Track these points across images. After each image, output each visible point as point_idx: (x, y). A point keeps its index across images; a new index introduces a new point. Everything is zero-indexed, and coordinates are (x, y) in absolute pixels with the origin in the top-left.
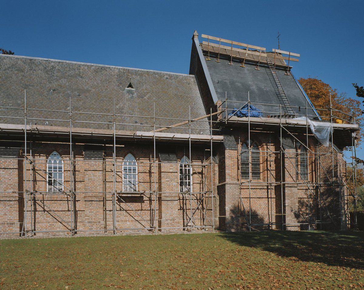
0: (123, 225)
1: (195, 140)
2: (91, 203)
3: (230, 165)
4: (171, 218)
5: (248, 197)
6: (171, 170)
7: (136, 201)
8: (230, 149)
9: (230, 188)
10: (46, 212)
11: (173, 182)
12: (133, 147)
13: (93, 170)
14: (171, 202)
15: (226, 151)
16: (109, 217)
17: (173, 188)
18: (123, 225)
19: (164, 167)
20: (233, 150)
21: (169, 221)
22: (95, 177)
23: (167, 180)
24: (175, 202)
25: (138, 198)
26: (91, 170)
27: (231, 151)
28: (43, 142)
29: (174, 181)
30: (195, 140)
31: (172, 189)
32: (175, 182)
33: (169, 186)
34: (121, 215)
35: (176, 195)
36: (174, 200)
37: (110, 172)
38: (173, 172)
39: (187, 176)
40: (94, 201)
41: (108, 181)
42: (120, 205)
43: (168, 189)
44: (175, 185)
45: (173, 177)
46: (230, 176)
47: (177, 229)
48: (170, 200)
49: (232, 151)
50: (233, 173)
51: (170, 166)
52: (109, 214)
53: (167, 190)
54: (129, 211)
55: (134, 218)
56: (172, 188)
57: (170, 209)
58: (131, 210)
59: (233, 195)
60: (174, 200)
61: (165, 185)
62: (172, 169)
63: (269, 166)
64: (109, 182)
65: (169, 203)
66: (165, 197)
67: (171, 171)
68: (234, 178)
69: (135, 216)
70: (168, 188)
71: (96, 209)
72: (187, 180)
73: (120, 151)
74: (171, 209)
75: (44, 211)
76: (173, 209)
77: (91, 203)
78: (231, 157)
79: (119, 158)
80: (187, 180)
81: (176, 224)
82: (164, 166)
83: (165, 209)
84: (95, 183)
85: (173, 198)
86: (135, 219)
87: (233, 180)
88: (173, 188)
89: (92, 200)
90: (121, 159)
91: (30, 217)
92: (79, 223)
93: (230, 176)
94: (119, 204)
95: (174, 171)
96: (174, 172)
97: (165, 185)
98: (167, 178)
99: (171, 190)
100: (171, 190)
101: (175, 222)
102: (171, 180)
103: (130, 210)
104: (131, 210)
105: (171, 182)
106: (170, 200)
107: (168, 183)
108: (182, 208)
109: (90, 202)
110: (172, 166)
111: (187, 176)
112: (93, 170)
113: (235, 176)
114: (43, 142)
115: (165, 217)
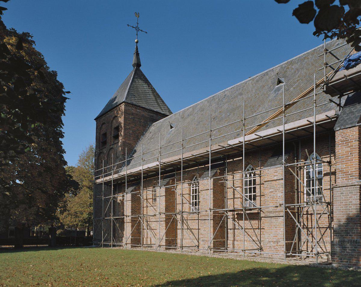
0: (241, 245)
1: (321, 123)
2: (204, 222)
3: (344, 155)
4: (275, 240)
5: (128, 223)
6: (275, 177)
7: (254, 218)
8: (343, 127)
9: (341, 193)
10: (189, 230)
11: (277, 192)
12: (251, 157)
13: (206, 190)
14: (275, 219)
15: (337, 134)
16: (230, 235)
17: (278, 200)
18: (241, 245)
19: (268, 175)
20: (350, 128)
21: (272, 243)
22: (207, 196)
23: (270, 190)
24: (279, 218)
25: (256, 215)
26: (205, 190)
27: (345, 131)
28: (187, 170)
29: (278, 191)
30: (321, 123)
31: (277, 202)
32: (280, 193)
33: (274, 199)
34: (241, 234)
35: (281, 209)
36: (278, 217)
37: (230, 189)
38: (278, 180)
39: (311, 181)
40: (206, 220)
41: (229, 198)
42: (238, 223)
43: (272, 203)
44: (279, 197)
45: (277, 186)
46: (345, 173)
47: (281, 255)
48: (274, 217)
49: (349, 130)
50: (351, 167)
51: (274, 172)
52: (230, 233)
53: (270, 204)
54: (247, 230)
55: (251, 238)
56: (276, 200)
57: (274, 228)
58: (249, 229)
59: (346, 205)
60: (278, 217)
61: (268, 198)
62: (276, 176)
63: (237, 181)
64: (230, 199)
65: (273, 220)
66: (268, 213)
67: (275, 178)
68: (351, 176)
69: (253, 236)
70: (272, 201)
71: (208, 228)
72: (195, 202)
73: (238, 164)
74: (275, 228)
75: (188, 229)
76: (277, 228)
77: (204, 222)
78: (346, 142)
79: (238, 172)
80: (195, 202)
81: (281, 247)
82: (267, 174)
83: (268, 228)
84: (207, 203)
85: (277, 213)
86: (252, 239)
87: (349, 179)
88: (278, 200)
89: (205, 219)
90: (239, 172)
91: (181, 234)
92: (249, 242)
93: (345, 173)
94: (238, 221)
95: (278, 178)
96: (280, 179)
97: (268, 198)
98: (270, 189)
99: (275, 203)
100: (275, 203)
101: (279, 245)
102: (275, 190)
103: (248, 229)
104: (249, 229)
105: (275, 193)
106: (274, 217)
107: (272, 194)
108: (305, 227)
109: (204, 221)
110: (276, 172)
111: (311, 181)
112: (206, 190)
113: (354, 171)
114: (187, 170)
115: (268, 238)
